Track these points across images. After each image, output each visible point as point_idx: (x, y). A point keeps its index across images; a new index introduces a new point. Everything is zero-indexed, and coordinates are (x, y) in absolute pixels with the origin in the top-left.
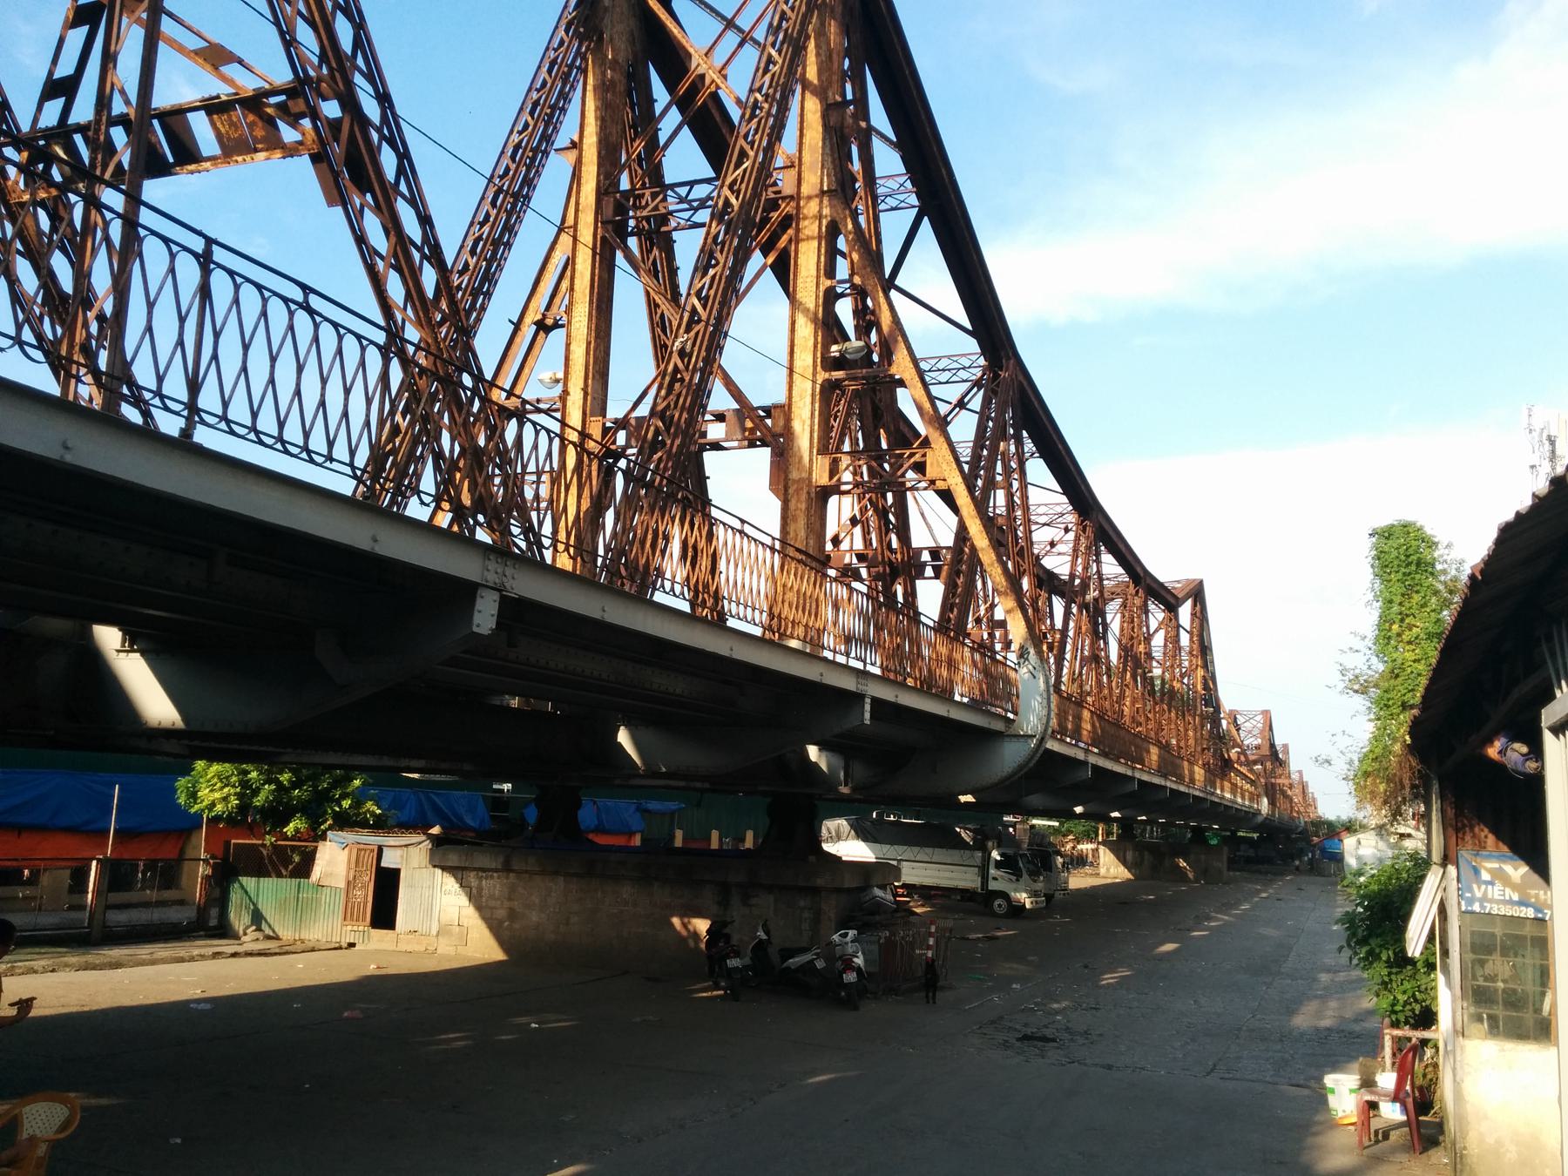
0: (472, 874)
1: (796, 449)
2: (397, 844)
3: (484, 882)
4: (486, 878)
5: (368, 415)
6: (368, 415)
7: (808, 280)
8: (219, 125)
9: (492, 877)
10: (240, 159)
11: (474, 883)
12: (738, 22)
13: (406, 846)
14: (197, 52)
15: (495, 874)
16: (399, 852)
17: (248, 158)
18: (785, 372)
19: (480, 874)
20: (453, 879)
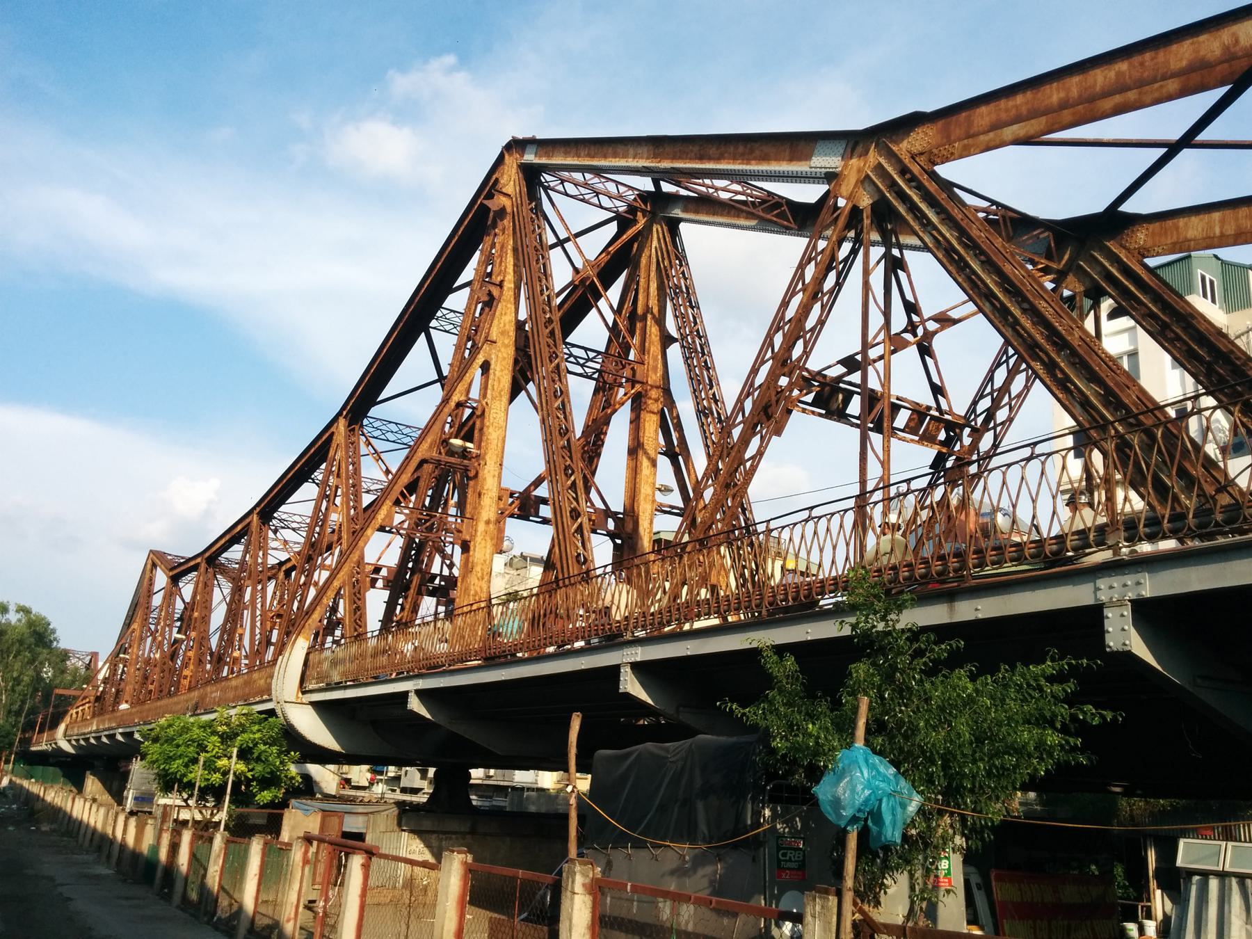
0: (434, 836)
1: (639, 546)
2: (365, 811)
3: (444, 843)
4: (446, 840)
5: (848, 554)
6: (848, 554)
7: (650, 439)
8: (931, 426)
9: (451, 839)
10: (926, 443)
11: (435, 843)
12: (562, 238)
13: (367, 813)
14: (943, 396)
15: (454, 836)
16: (361, 819)
17: (930, 445)
18: (505, 464)
19: (441, 836)
20: (418, 841)
